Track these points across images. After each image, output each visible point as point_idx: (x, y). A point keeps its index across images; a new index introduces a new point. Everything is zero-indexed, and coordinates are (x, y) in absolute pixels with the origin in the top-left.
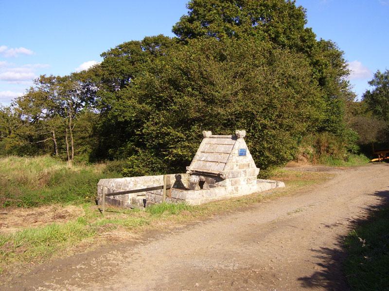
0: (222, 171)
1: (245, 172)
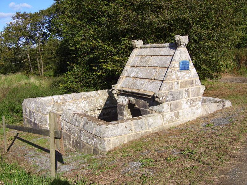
0: (157, 92)
1: (188, 91)
